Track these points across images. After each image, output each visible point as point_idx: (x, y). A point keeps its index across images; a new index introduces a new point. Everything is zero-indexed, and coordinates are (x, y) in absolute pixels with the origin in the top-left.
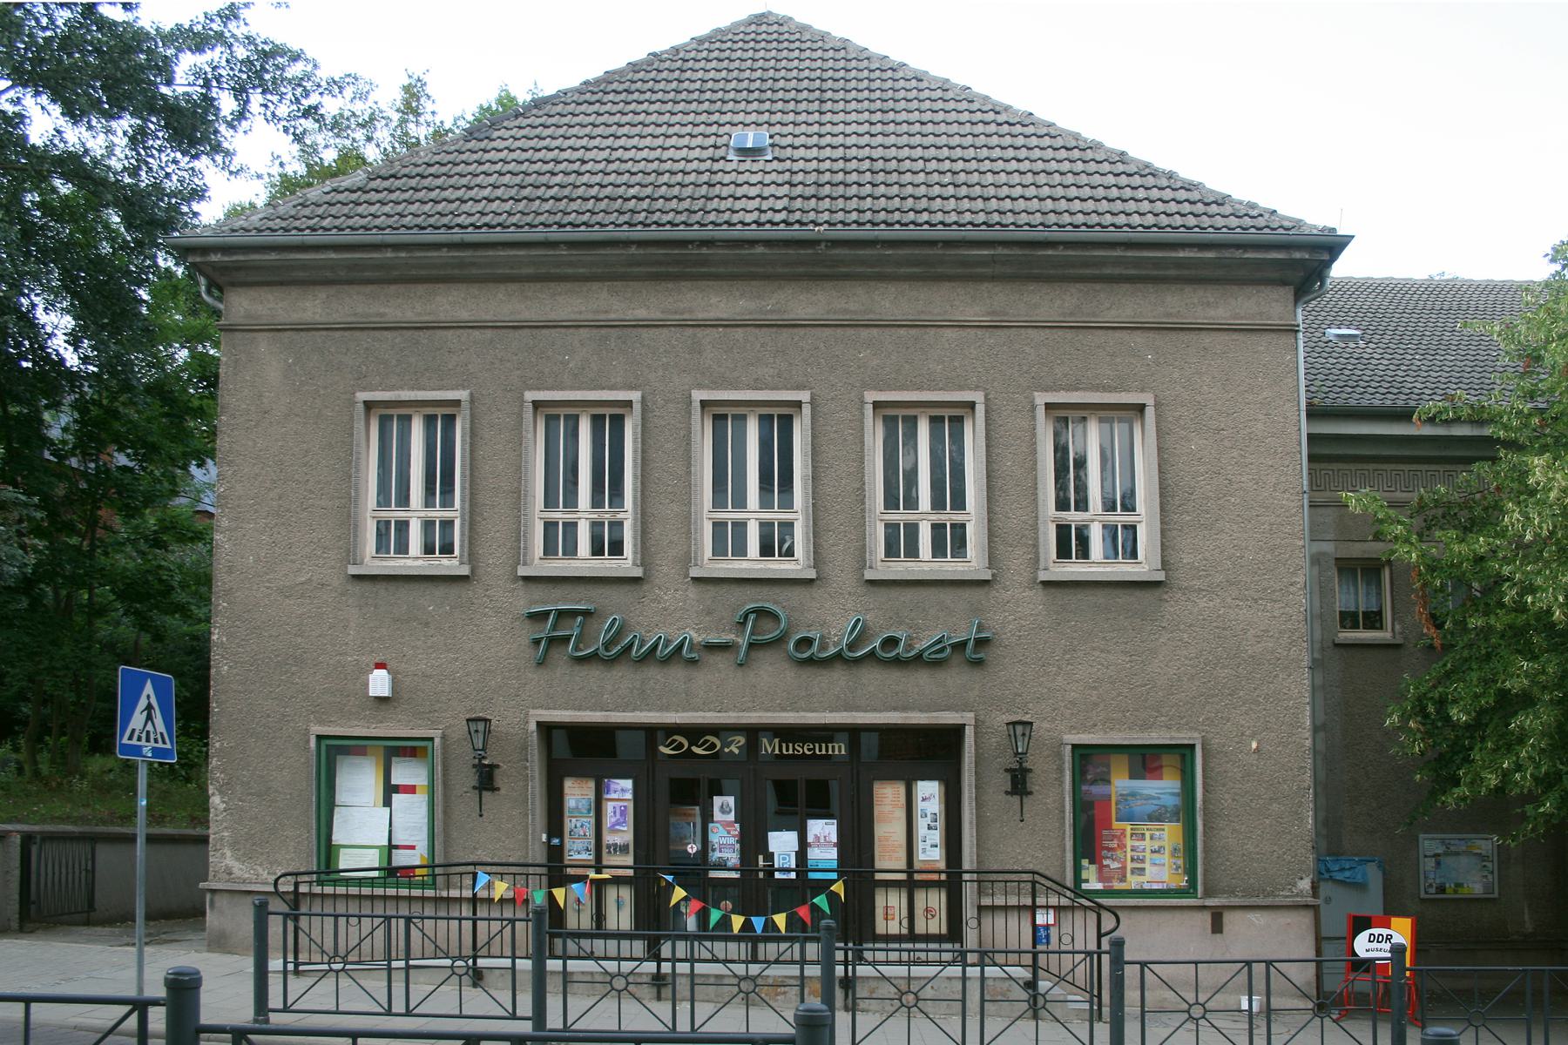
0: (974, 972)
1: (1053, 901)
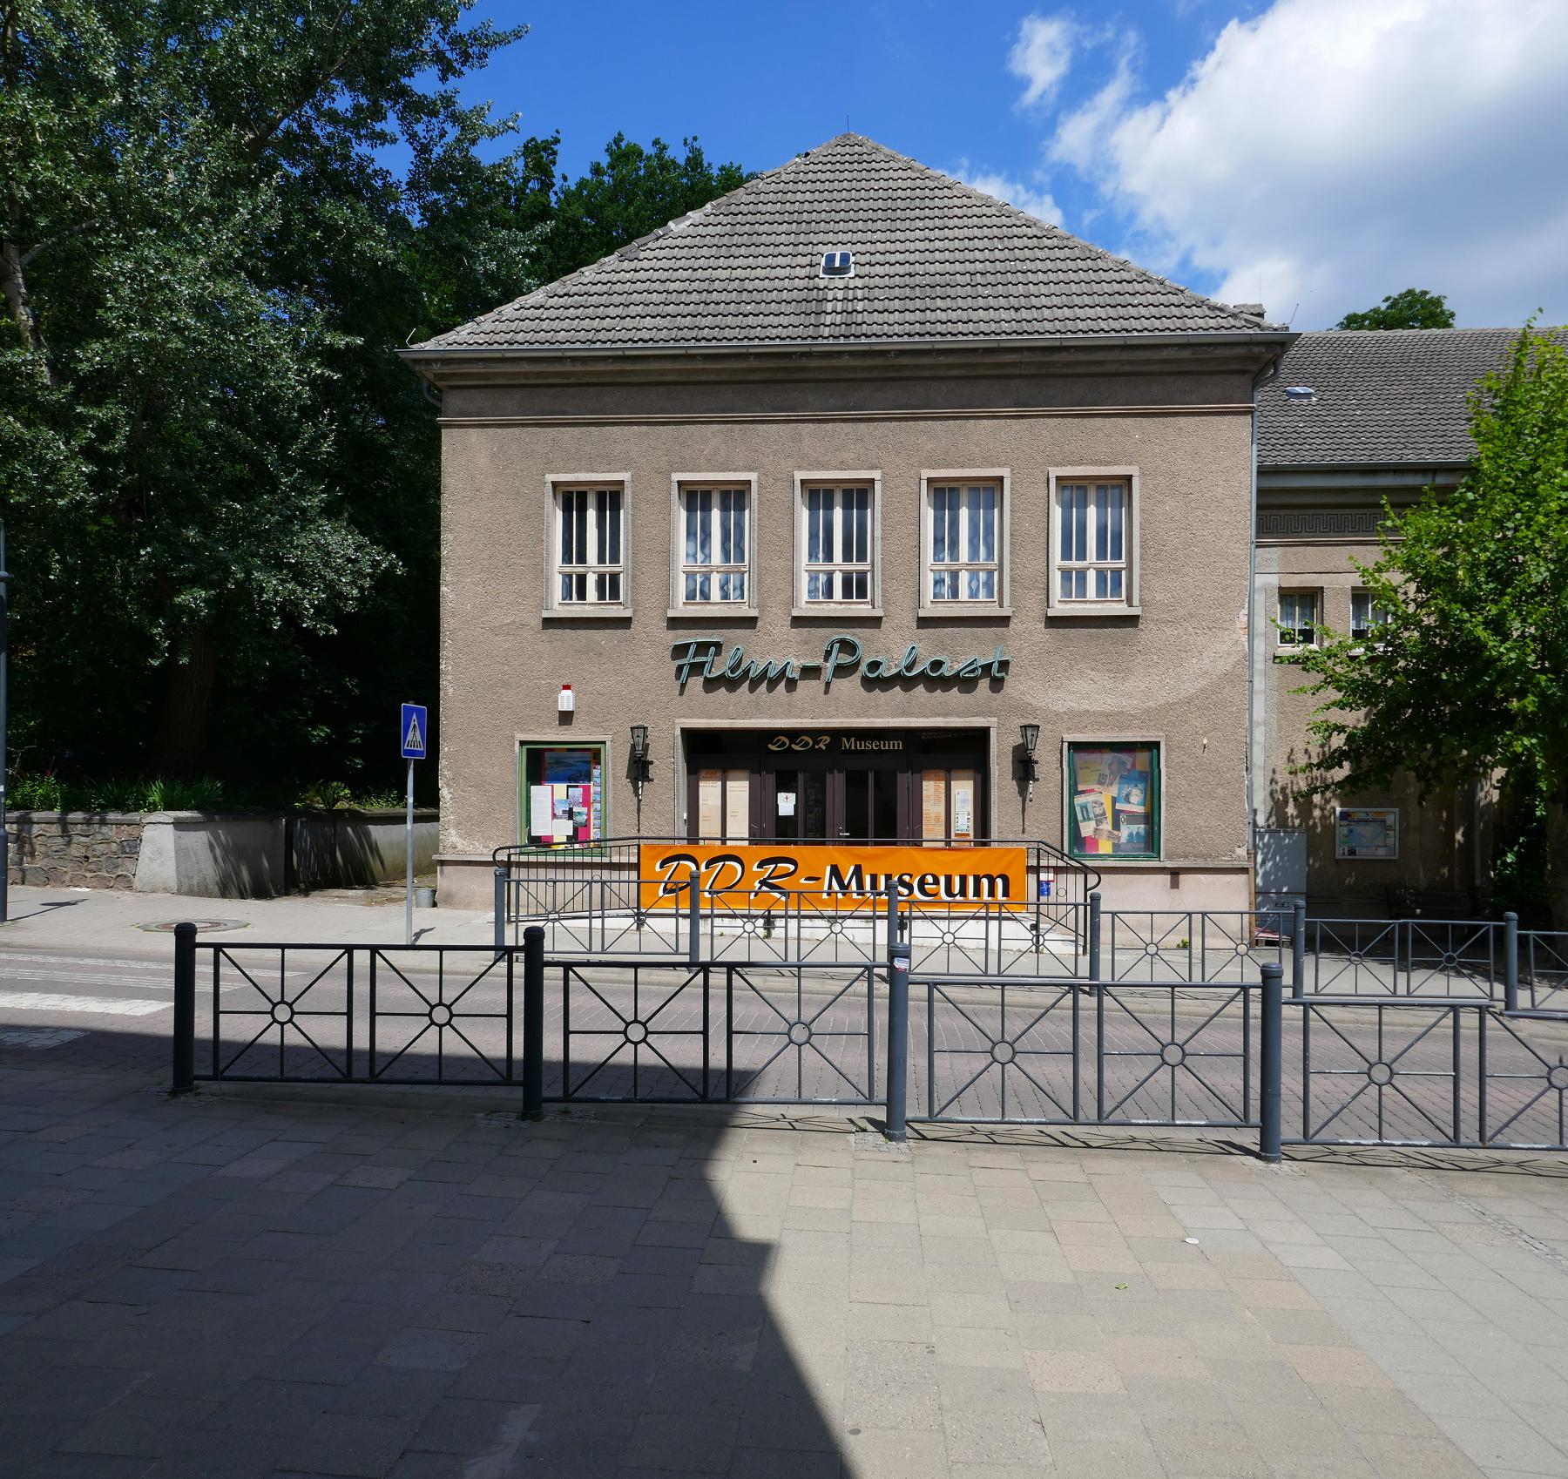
0: (597, 923)
1: (1053, 862)
